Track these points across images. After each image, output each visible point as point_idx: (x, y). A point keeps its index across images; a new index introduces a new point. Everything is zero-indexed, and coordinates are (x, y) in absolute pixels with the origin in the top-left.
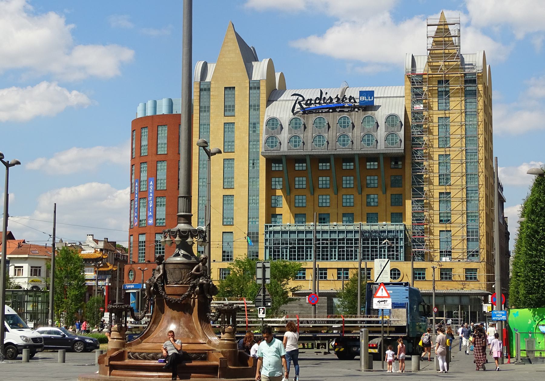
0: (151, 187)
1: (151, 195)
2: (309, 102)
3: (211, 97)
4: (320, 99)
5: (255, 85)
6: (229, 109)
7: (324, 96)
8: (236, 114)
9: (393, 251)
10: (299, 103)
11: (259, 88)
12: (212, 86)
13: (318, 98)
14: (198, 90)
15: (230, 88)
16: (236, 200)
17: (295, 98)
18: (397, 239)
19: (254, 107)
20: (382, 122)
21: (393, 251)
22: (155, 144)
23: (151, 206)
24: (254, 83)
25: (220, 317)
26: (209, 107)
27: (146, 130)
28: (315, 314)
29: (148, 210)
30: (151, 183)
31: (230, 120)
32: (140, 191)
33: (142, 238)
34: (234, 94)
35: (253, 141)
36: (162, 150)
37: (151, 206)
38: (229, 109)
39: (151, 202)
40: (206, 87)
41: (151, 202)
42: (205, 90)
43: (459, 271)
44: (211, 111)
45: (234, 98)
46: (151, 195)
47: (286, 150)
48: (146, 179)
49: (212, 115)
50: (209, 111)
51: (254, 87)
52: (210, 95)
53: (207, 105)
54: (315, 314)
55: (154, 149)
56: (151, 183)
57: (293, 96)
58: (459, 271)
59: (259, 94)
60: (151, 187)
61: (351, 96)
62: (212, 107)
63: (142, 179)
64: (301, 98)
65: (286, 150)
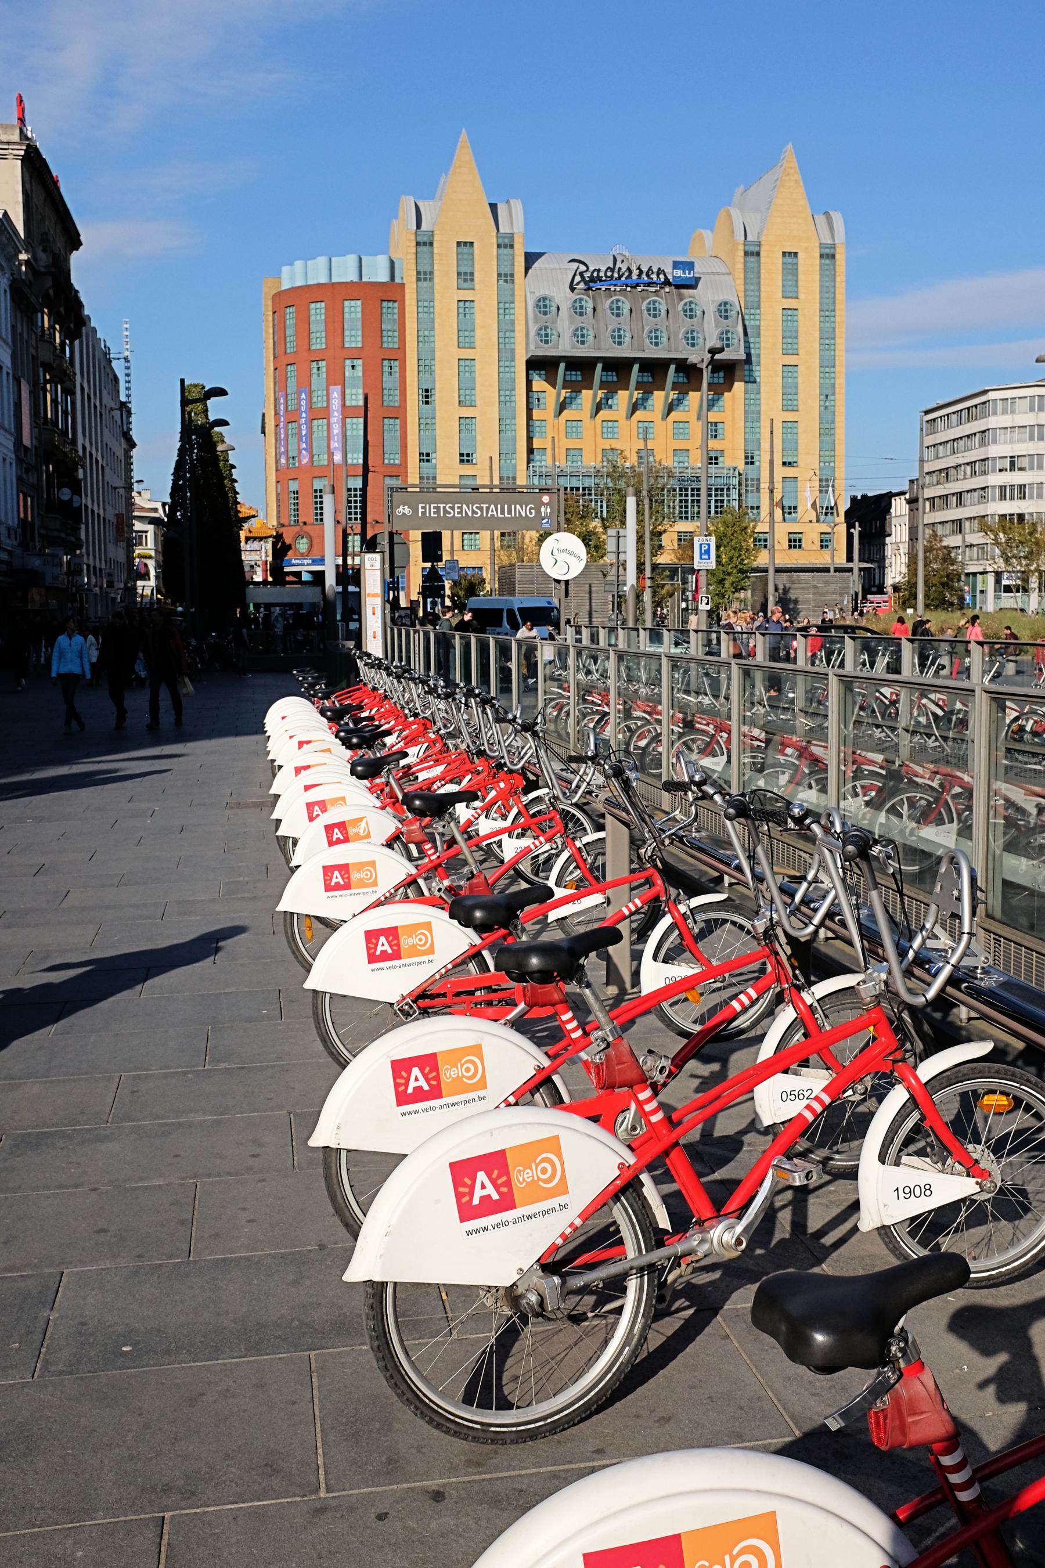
0: (303, 403)
1: (304, 415)
2: (595, 274)
3: (436, 257)
4: (612, 270)
5: (506, 241)
6: (466, 277)
7: (619, 265)
8: (477, 287)
9: (722, 495)
10: (581, 274)
11: (512, 246)
12: (436, 238)
13: (609, 268)
14: (414, 244)
15: (465, 243)
16: (801, 427)
17: (575, 265)
18: (728, 489)
19: (506, 277)
20: (711, 310)
21: (722, 495)
22: (340, 330)
23: (304, 433)
24: (504, 238)
25: (73, 539)
26: (432, 273)
27: (291, 309)
28: (345, 556)
29: (300, 439)
30: (303, 396)
31: (466, 295)
32: (286, 410)
33: (294, 486)
34: (472, 254)
35: (505, 330)
36: (319, 343)
37: (304, 433)
38: (466, 277)
39: (304, 427)
40: (425, 239)
41: (304, 427)
42: (425, 244)
43: (811, 536)
44: (436, 280)
45: (473, 260)
46: (304, 415)
47: (568, 347)
48: (294, 390)
49: (436, 287)
50: (431, 280)
51: (506, 244)
52: (432, 253)
53: (428, 269)
54: (345, 556)
55: (339, 340)
56: (303, 396)
57: (530, 271)
58: (811, 536)
59: (513, 255)
60: (303, 403)
61: (659, 269)
62: (436, 273)
63: (289, 391)
64: (583, 268)
65: (568, 347)
